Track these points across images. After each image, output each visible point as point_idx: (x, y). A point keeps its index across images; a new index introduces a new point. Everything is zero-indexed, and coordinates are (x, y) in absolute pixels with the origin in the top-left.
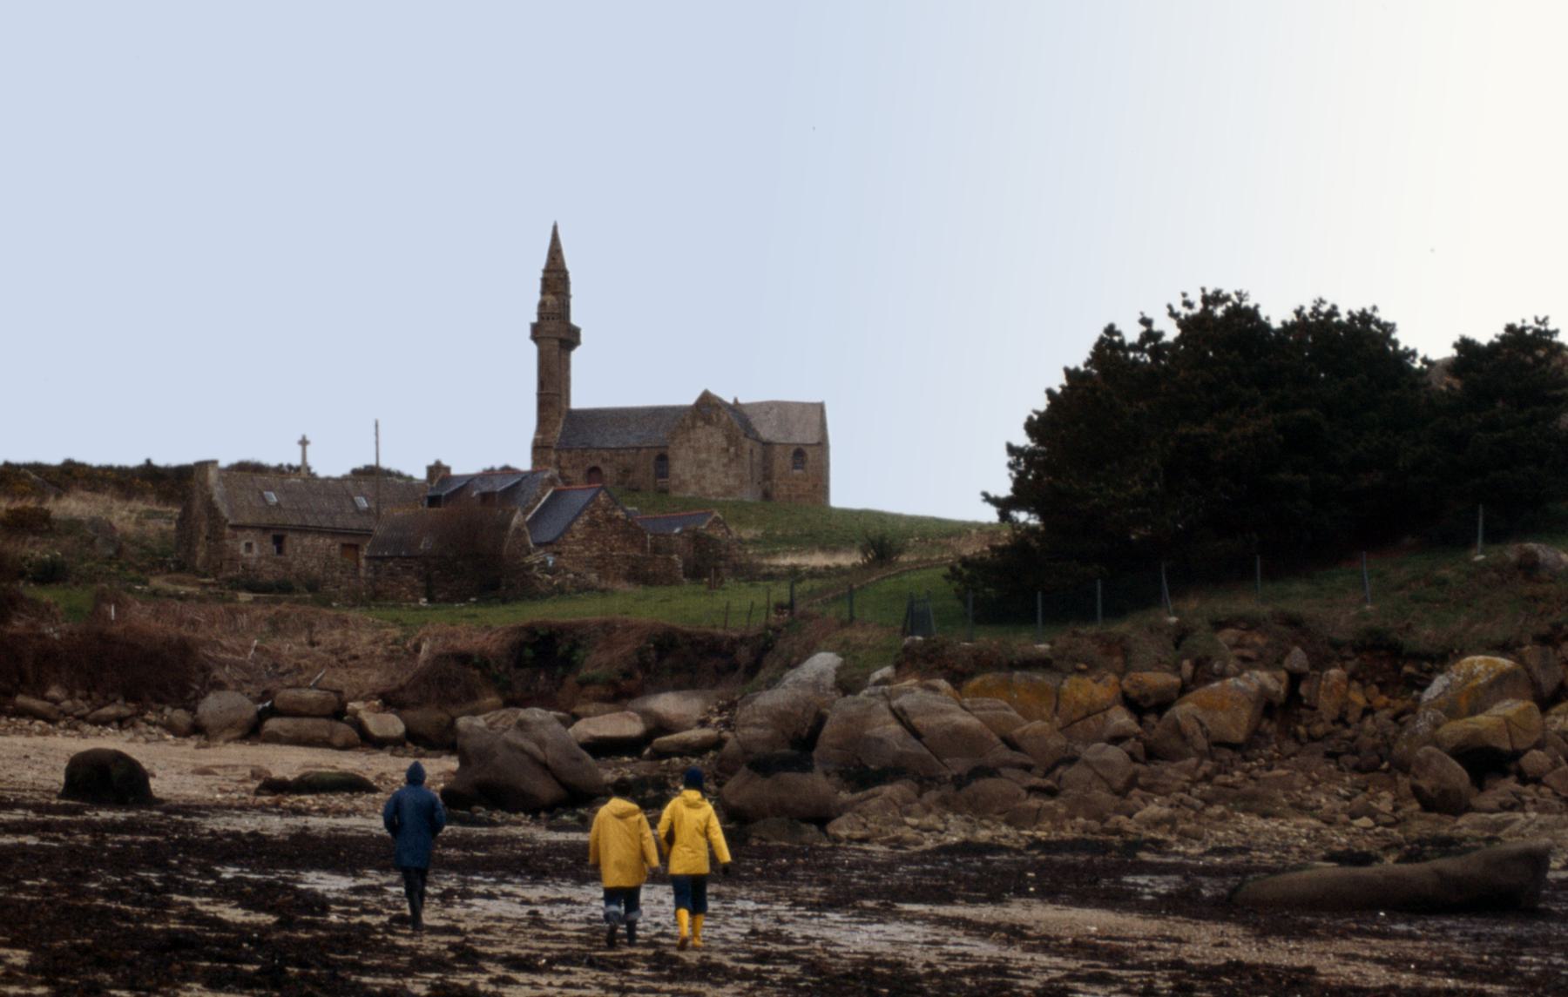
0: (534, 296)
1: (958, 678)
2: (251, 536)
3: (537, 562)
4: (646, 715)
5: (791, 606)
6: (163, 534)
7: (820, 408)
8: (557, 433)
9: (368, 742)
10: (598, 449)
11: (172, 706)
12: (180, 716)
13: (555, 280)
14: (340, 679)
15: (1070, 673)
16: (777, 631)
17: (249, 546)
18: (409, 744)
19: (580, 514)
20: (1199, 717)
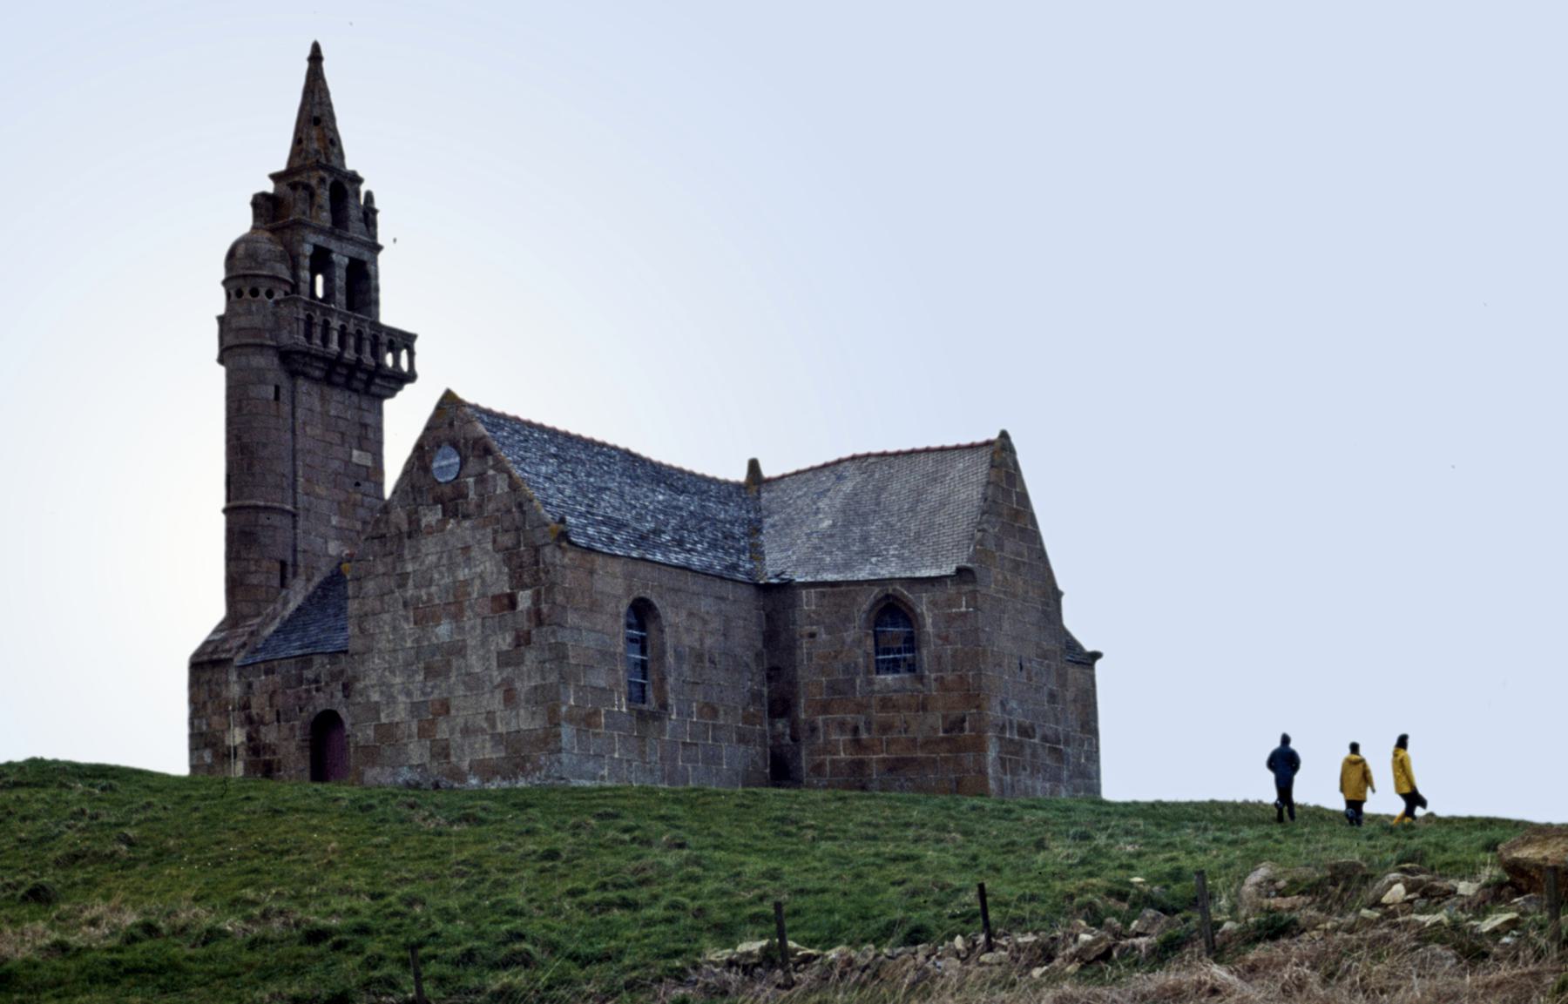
0: (305, 66)
7: (1000, 452)
13: (316, 57)
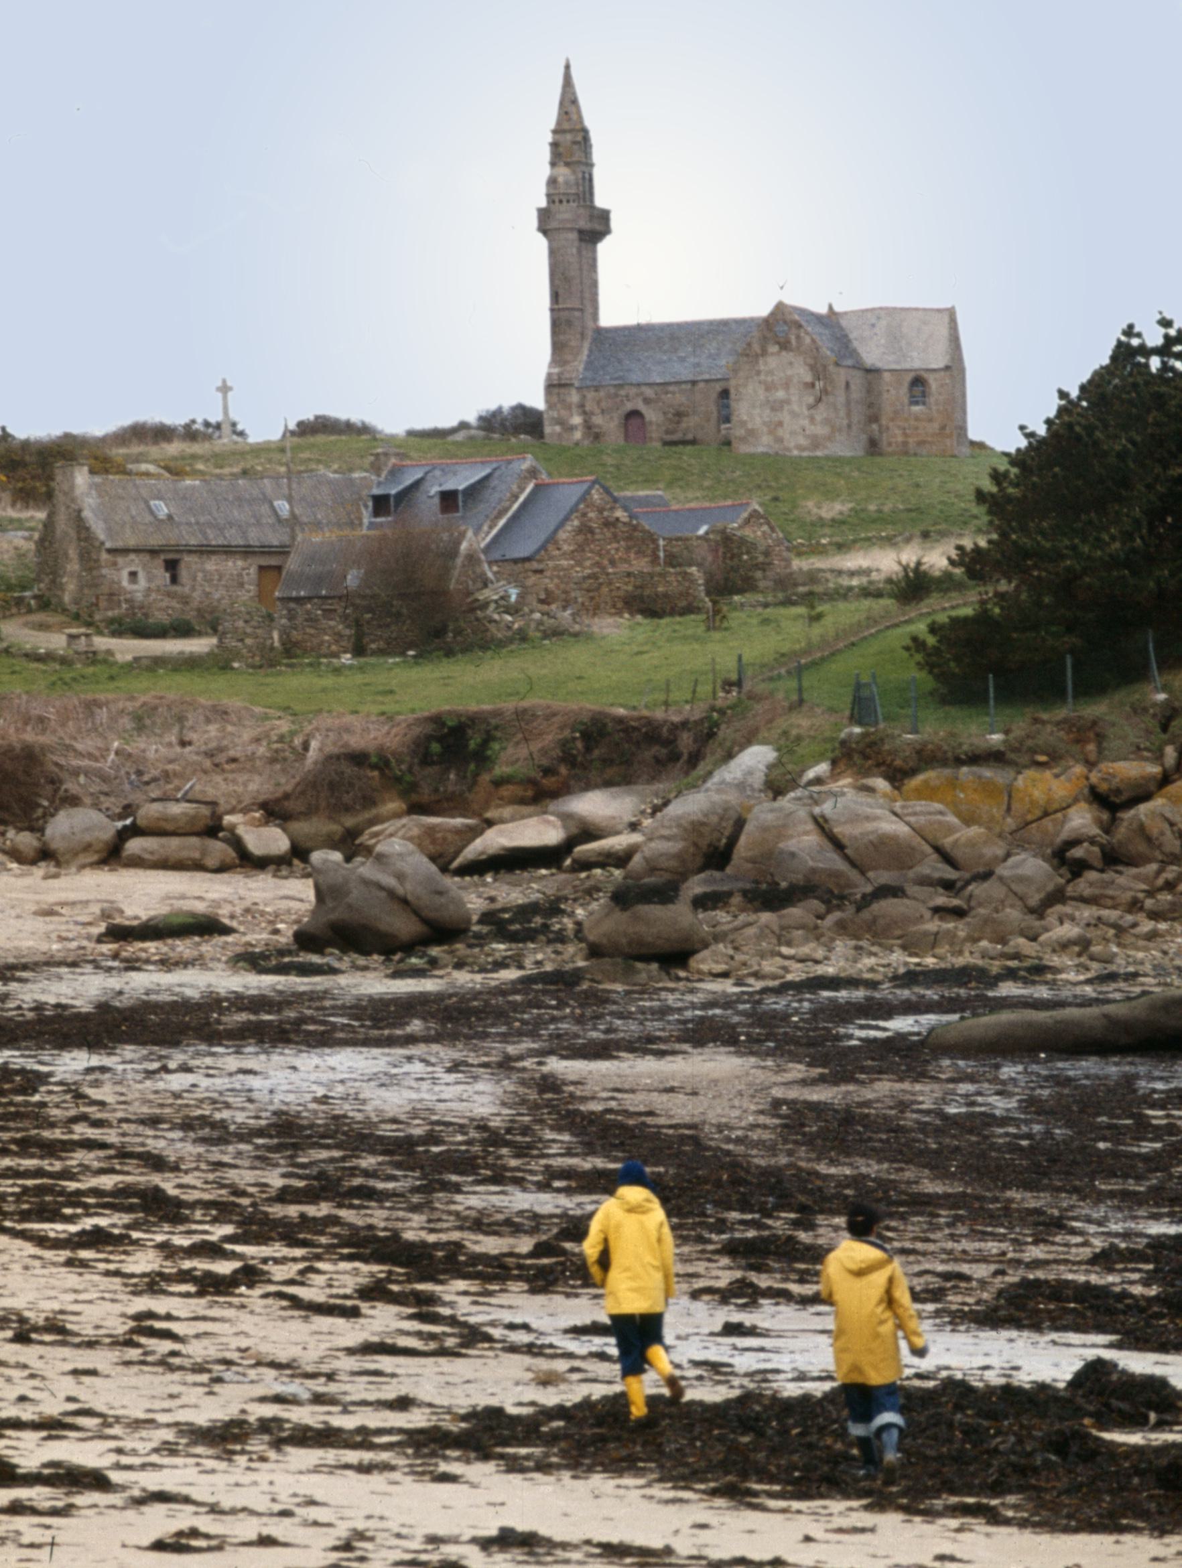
1: (897, 777)
2: (134, 563)
3: (495, 597)
4: (566, 817)
5: (739, 684)
6: (20, 555)
7: (951, 314)
8: (577, 368)
9: (249, 862)
10: (639, 385)
11: (16, 828)
12: (26, 840)
13: (567, 67)
14: (217, 788)
15: (1026, 767)
16: (722, 712)
17: (133, 575)
18: (296, 862)
19: (567, 519)
20: (1168, 815)
